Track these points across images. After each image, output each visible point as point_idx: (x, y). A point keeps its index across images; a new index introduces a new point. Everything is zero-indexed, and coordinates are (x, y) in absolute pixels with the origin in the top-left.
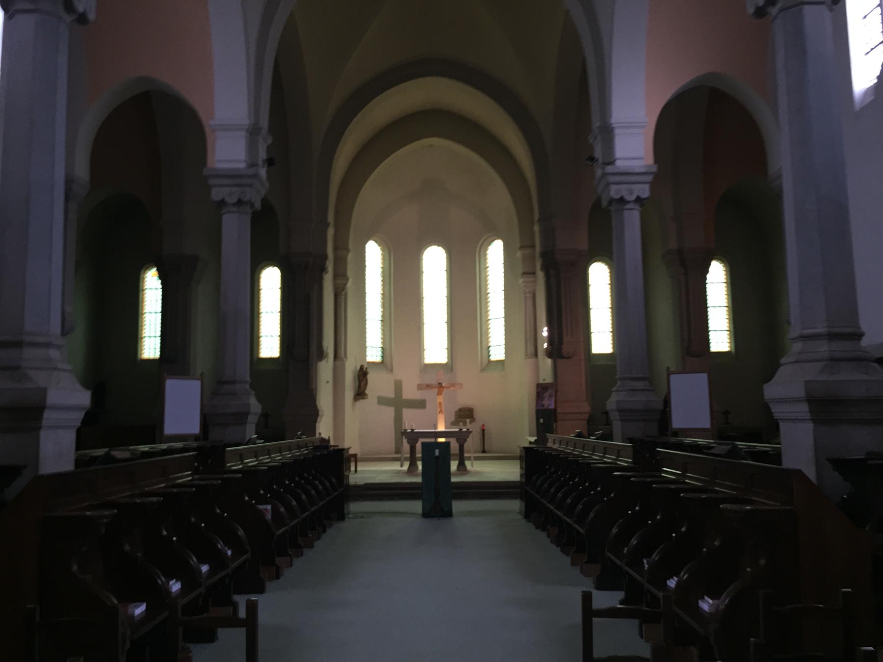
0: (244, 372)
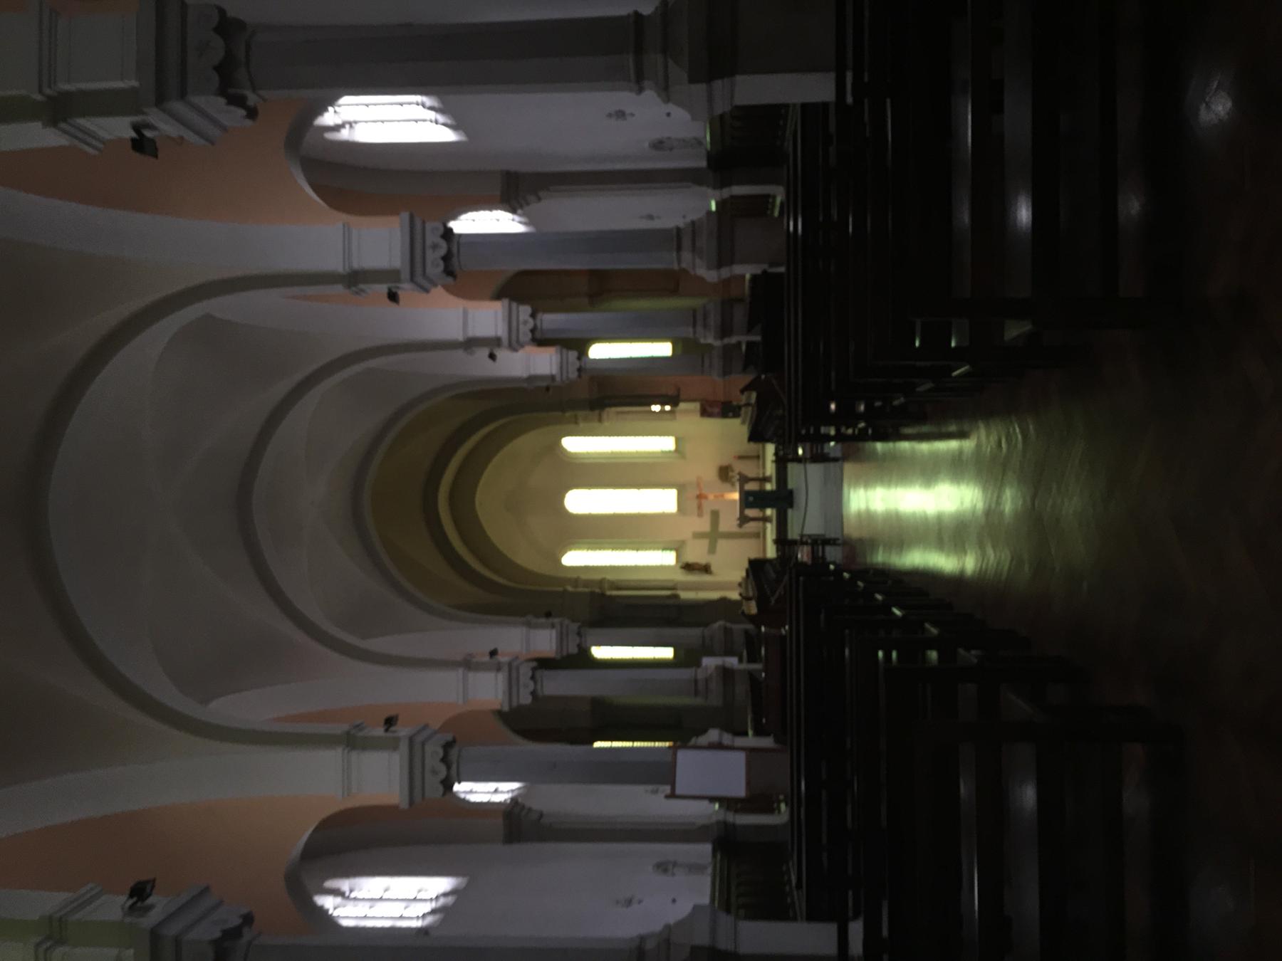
0: (685, 674)
